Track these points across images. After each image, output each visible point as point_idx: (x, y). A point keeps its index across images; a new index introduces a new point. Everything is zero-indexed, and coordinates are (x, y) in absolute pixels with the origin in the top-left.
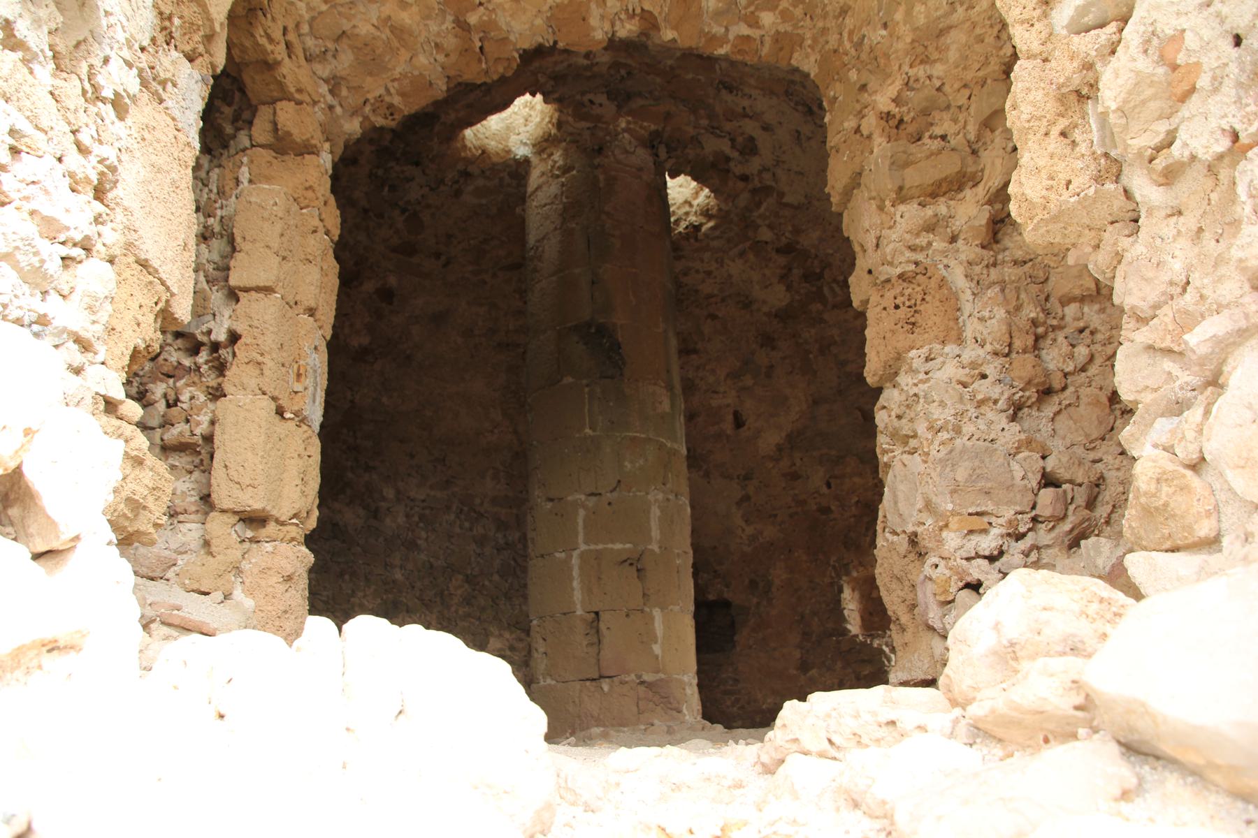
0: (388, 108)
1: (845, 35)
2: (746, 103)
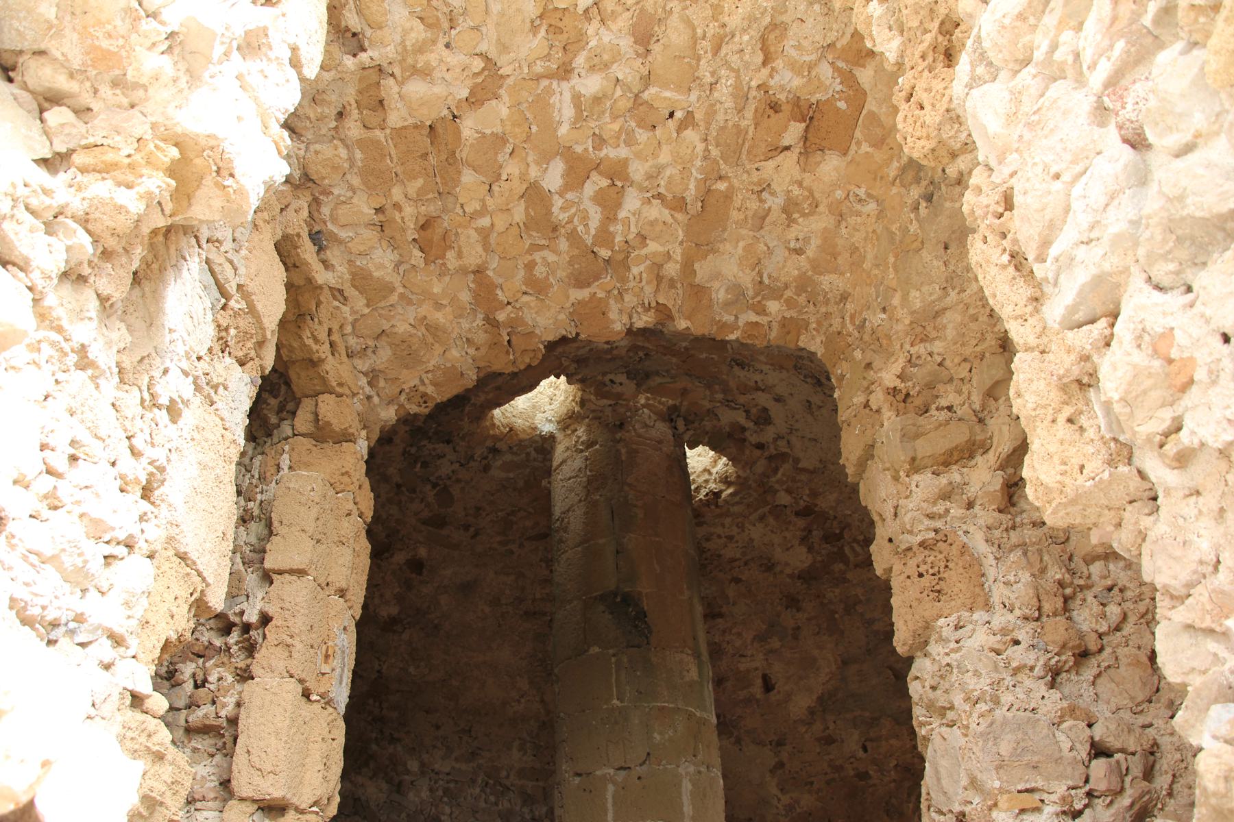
1: (847, 318)
2: (758, 377)
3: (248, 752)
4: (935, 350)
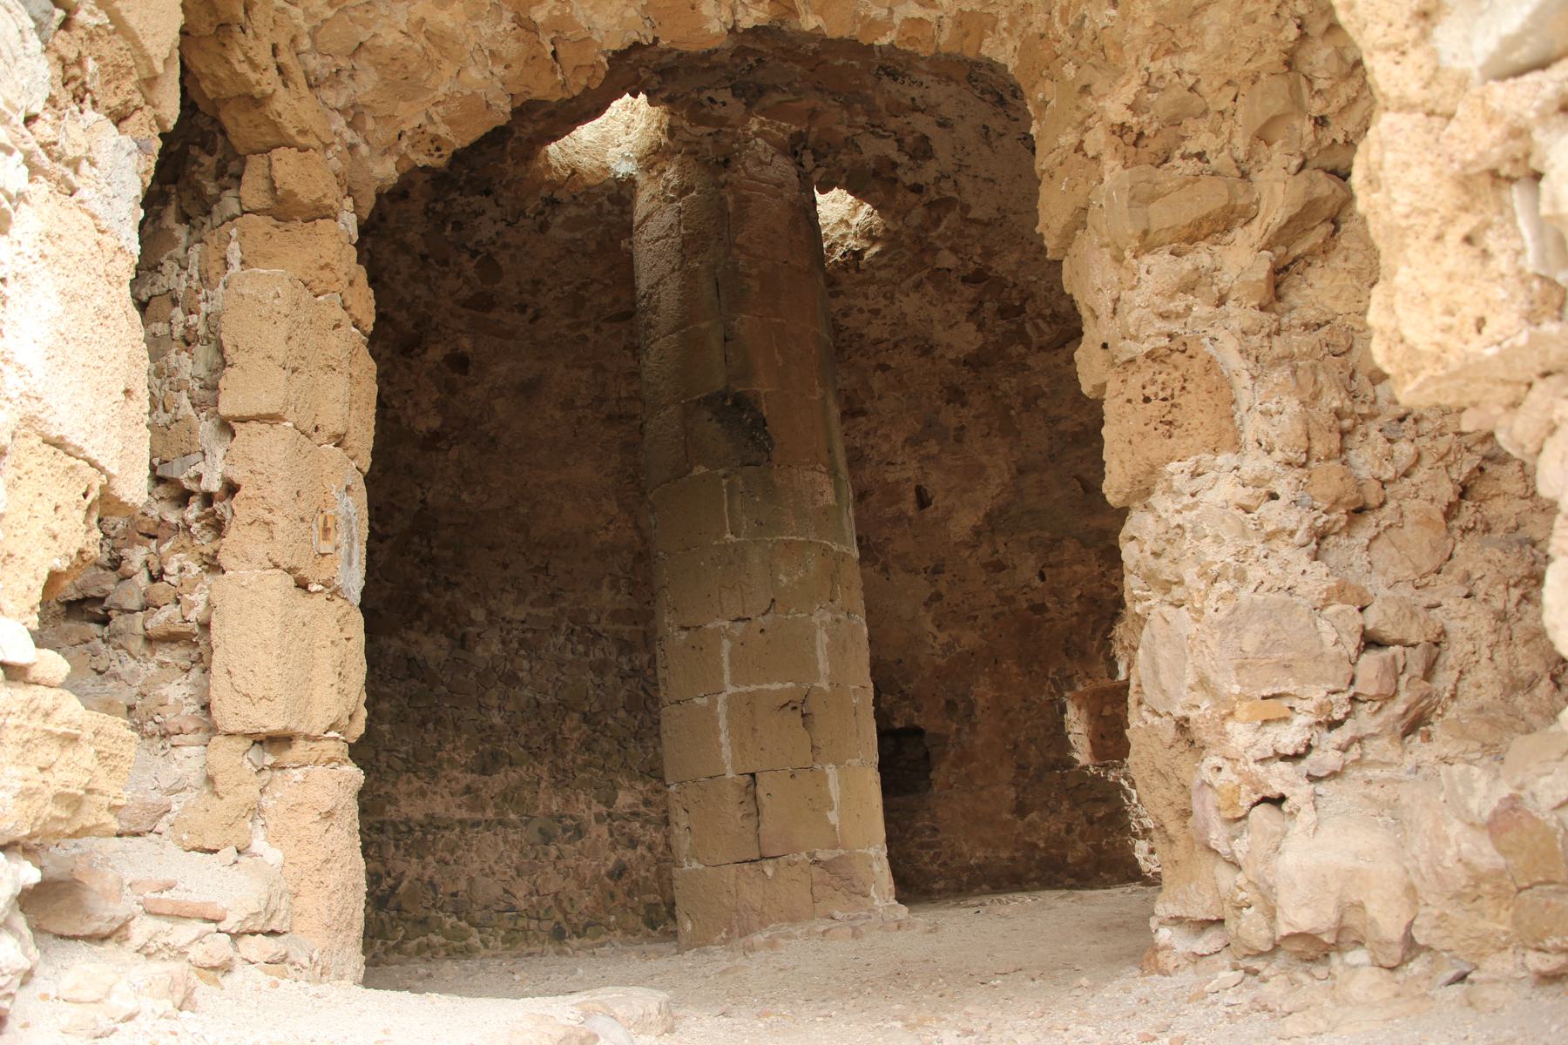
0: (432, 142)
1: (1056, 14)
2: (915, 92)
3: (229, 672)
4: (1186, 67)
